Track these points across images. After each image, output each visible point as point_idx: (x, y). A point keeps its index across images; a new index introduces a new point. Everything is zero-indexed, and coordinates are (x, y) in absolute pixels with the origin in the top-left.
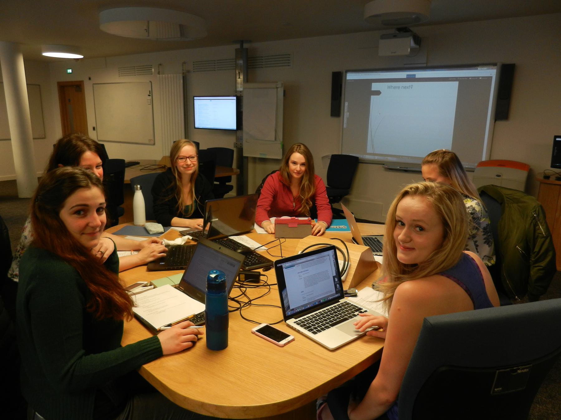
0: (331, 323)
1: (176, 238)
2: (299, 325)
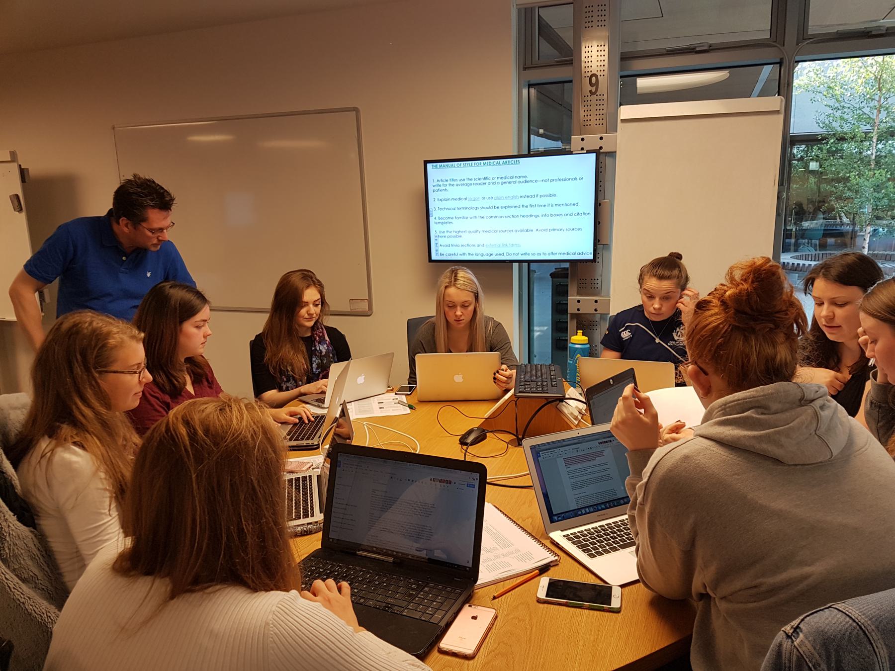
0: (621, 543)
1: (297, 590)
2: (570, 540)
